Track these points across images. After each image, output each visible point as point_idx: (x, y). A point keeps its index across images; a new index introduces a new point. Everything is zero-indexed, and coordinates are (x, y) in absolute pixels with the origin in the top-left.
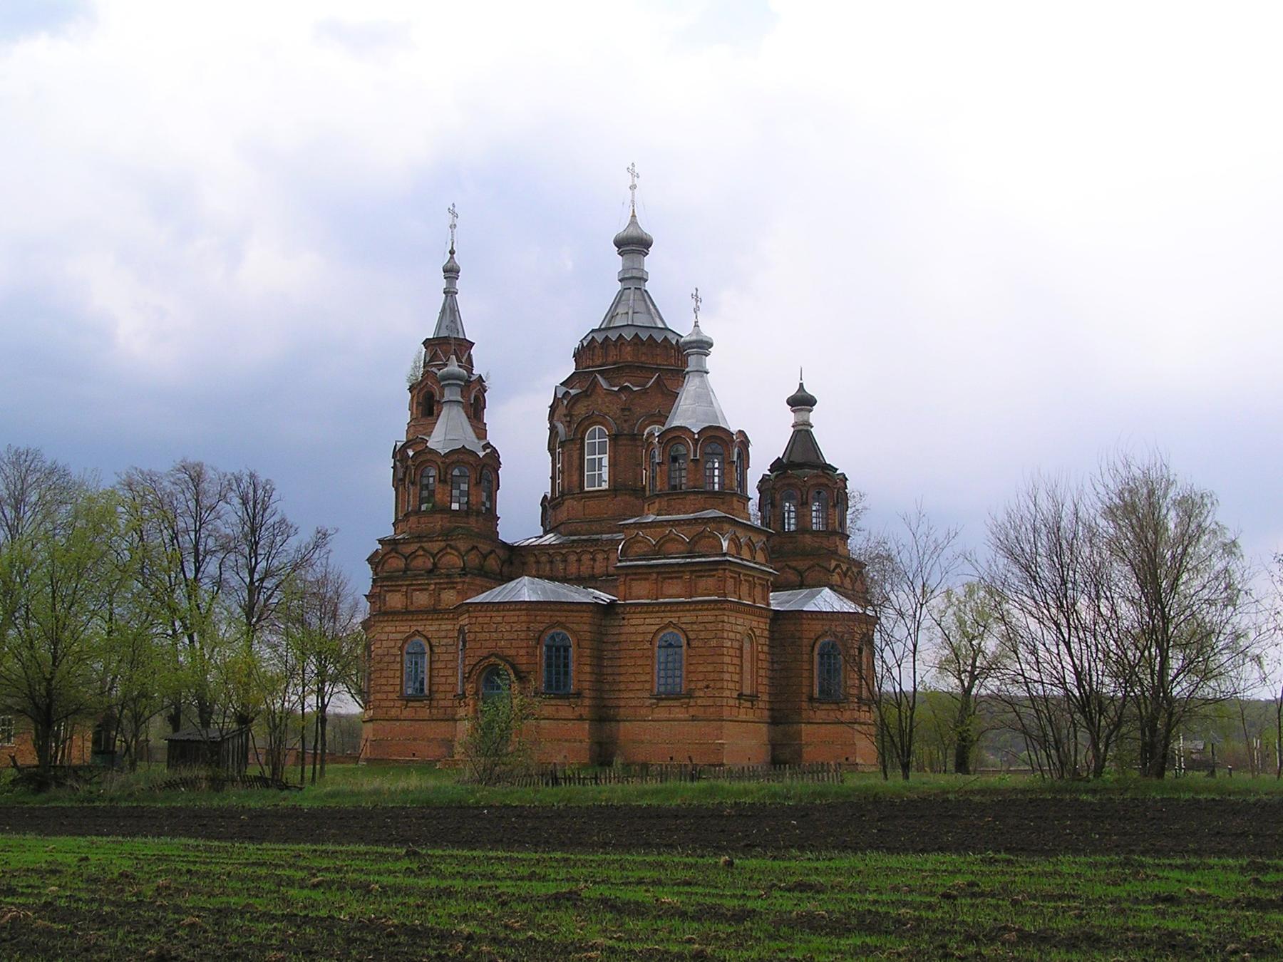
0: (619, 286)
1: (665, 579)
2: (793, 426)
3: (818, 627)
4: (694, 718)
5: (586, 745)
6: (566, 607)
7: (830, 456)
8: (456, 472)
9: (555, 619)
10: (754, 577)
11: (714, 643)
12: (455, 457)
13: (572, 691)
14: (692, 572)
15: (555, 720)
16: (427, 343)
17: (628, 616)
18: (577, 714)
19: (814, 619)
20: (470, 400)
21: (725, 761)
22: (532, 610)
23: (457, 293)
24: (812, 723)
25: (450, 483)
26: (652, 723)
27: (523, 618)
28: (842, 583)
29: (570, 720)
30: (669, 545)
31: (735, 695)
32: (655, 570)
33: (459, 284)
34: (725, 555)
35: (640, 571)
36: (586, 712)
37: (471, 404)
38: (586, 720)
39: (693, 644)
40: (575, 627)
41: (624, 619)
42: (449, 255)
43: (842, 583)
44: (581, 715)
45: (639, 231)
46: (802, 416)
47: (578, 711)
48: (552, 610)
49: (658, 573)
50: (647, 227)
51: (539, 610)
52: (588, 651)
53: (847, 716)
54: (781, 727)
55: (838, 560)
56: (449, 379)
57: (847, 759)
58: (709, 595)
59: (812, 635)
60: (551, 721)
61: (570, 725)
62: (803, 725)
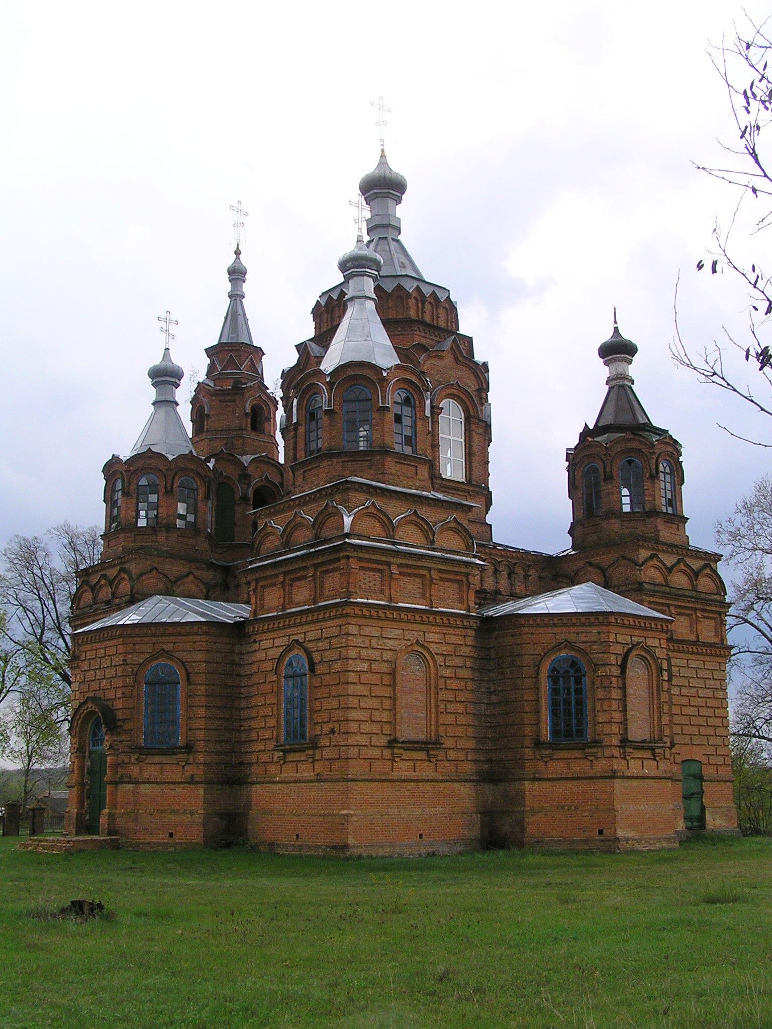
2: (607, 384)
3: (547, 637)
4: (319, 779)
5: (198, 819)
8: (143, 481)
10: (429, 569)
11: (337, 666)
12: (140, 464)
13: (180, 744)
14: (316, 566)
15: (157, 783)
16: (210, 351)
18: (188, 774)
19: (539, 626)
21: (351, 841)
23: (244, 297)
25: (134, 495)
27: (121, 649)
28: (666, 580)
30: (297, 533)
31: (384, 741)
33: (246, 287)
34: (347, 535)
35: (267, 573)
36: (199, 772)
37: (246, 414)
38: (200, 783)
39: (320, 669)
40: (186, 657)
41: (255, 641)
42: (235, 256)
43: (666, 580)
44: (192, 777)
45: (387, 171)
46: (620, 367)
47: (190, 770)
48: (154, 635)
49: (285, 573)
50: (398, 167)
51: (138, 636)
52: (203, 687)
53: (601, 766)
54: (502, 786)
55: (653, 549)
56: (165, 375)
57: (601, 832)
58: (447, 608)
60: (377, 783)
61: (179, 790)
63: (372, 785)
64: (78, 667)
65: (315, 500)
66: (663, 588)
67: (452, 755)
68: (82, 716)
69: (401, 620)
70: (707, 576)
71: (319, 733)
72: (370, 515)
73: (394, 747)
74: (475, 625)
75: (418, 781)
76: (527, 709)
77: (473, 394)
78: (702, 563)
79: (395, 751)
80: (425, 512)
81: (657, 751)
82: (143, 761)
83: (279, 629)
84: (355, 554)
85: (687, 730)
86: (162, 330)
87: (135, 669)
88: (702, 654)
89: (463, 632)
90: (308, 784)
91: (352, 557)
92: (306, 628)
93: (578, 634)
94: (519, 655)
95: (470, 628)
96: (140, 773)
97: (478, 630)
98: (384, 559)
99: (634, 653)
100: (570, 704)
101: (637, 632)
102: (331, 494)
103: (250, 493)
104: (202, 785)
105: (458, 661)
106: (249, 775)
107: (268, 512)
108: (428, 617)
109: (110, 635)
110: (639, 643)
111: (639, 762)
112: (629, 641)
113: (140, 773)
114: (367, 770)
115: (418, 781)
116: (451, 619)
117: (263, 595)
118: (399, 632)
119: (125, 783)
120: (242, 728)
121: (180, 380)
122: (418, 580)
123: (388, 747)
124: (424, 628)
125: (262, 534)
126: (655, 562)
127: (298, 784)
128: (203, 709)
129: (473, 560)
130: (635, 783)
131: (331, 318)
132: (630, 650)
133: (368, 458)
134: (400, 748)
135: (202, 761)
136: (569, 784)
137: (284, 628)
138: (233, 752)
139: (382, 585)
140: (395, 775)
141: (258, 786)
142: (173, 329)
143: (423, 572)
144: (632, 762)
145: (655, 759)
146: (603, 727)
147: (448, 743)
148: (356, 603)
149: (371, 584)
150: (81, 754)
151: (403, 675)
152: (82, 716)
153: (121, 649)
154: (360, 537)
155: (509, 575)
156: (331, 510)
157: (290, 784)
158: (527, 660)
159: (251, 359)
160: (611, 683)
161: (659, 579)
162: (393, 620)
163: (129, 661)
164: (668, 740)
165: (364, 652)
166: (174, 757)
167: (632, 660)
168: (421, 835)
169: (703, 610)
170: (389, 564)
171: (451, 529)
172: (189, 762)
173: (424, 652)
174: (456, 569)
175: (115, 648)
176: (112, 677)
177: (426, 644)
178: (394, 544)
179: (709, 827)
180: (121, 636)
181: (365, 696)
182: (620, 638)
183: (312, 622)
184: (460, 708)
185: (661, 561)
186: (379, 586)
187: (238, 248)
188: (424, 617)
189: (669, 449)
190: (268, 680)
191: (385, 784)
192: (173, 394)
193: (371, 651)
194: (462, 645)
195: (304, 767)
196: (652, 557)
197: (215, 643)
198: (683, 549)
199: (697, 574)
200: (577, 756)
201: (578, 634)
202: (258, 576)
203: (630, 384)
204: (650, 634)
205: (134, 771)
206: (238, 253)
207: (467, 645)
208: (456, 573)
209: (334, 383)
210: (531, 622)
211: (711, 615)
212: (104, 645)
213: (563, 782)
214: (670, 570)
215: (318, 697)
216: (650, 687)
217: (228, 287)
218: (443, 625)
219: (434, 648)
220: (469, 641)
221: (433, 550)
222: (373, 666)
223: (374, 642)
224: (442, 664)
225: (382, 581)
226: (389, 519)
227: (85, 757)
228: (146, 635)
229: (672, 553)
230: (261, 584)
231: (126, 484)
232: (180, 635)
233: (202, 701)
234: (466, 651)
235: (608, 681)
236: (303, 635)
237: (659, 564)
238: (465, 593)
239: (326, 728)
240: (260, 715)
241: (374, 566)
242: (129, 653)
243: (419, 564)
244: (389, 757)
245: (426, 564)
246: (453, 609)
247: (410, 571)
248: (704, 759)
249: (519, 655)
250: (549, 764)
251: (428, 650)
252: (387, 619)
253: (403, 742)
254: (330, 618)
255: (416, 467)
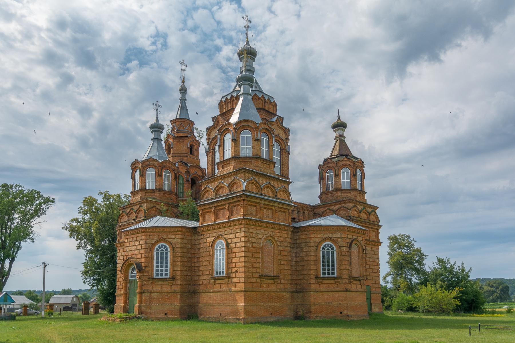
0: (335, 141)
1: (218, 210)
6: (166, 229)
7: (355, 152)
9: (160, 237)
10: (275, 206)
14: (229, 204)
17: (203, 233)
20: (187, 146)
22: (148, 232)
24: (318, 292)
26: (213, 293)
27: (144, 237)
28: (359, 216)
29: (169, 293)
31: (257, 275)
32: (213, 205)
36: (178, 290)
38: (178, 293)
40: (172, 241)
41: (201, 235)
43: (359, 216)
51: (151, 232)
55: (355, 203)
57: (341, 313)
59: (317, 240)
60: (254, 293)
61: (169, 296)
62: (312, 293)
63: (252, 293)
64: (124, 246)
65: (229, 177)
66: (358, 219)
67: (283, 281)
68: (126, 265)
69: (264, 227)
70: (373, 215)
71: (231, 272)
72: (252, 183)
73: (261, 278)
74: (291, 230)
75: (270, 292)
76: (312, 264)
77: (285, 140)
78: (371, 210)
79: (262, 279)
80: (273, 183)
81: (361, 281)
82: (153, 284)
83: (212, 229)
84: (247, 199)
85: (371, 274)
86: (155, 109)
87: (150, 246)
88: (371, 245)
89: (287, 232)
90: (225, 293)
91: (246, 200)
92: (225, 229)
93: (333, 234)
94: (309, 242)
95: (290, 231)
96: (152, 289)
97: (292, 232)
98: (258, 201)
99: (354, 242)
100: (329, 262)
101: (354, 234)
102: (236, 174)
103: (190, 179)
104: (179, 294)
105: (285, 244)
106: (199, 289)
107: (207, 182)
108: (274, 225)
109: (139, 231)
110: (355, 239)
111: (355, 285)
112: (352, 237)
113: (152, 289)
114: (251, 287)
115: (270, 292)
116: (283, 227)
117: (205, 216)
118: (263, 231)
119: (146, 293)
120: (195, 270)
121: (163, 130)
122: (270, 211)
123: (259, 278)
124: (273, 230)
125: (205, 191)
126: (355, 208)
127: (221, 293)
128: (180, 262)
129: (291, 204)
130: (354, 293)
131: (227, 107)
132: (352, 241)
133: (251, 160)
134: (264, 278)
135: (179, 283)
136: (329, 293)
137: (215, 229)
138: (192, 280)
139: (257, 212)
140: (261, 289)
141: (203, 294)
142: (159, 109)
143: (272, 208)
144: (353, 285)
145: (361, 284)
146: (342, 271)
147: (282, 277)
148: (247, 219)
149: (253, 212)
150: (125, 281)
151: (264, 249)
152: (126, 265)
153: (144, 237)
154: (249, 192)
155: (298, 212)
156: (236, 181)
157: (217, 293)
158: (312, 244)
159: (189, 126)
160: (346, 254)
161: (357, 215)
162: (262, 226)
163: (147, 242)
164: (365, 277)
165: (250, 239)
166: (167, 282)
167: (353, 245)
168: (271, 313)
169: (372, 228)
170: (259, 204)
171: (283, 191)
172: (173, 284)
173: (273, 240)
174: (284, 207)
175: (141, 237)
176: (140, 249)
177: (273, 237)
178: (262, 195)
179: (373, 311)
180: (144, 232)
181: (250, 257)
182: (349, 236)
183: (228, 227)
184: (286, 263)
185: (357, 208)
186: (255, 212)
187: (183, 80)
188: (273, 225)
189: (360, 165)
190: (207, 251)
191: (258, 293)
192: (160, 136)
193: (253, 239)
194: (286, 238)
195: (224, 286)
196: (354, 207)
197: (184, 235)
198: (364, 203)
199: (370, 214)
200: (332, 283)
201: (333, 234)
202: (203, 208)
203: (344, 139)
204: (359, 235)
205: (150, 288)
206: (183, 82)
207: (288, 238)
208: (285, 209)
209: (236, 128)
210: (314, 229)
211: (374, 230)
212: (136, 236)
213: (327, 293)
214: (360, 212)
215: (230, 257)
216: (359, 256)
217: (180, 96)
218: (280, 229)
219: (276, 238)
220: (289, 236)
221: (276, 199)
222: (253, 245)
223: (254, 235)
224: (279, 245)
225: (257, 210)
226: (260, 185)
227: (127, 282)
228: (155, 232)
229: (361, 205)
230: (204, 211)
231: (142, 171)
232: (170, 232)
233: (179, 259)
234: (288, 240)
235: (345, 253)
236: (223, 232)
237: (356, 209)
238: (288, 217)
239: (234, 270)
240: (204, 265)
241: (254, 204)
242: (147, 239)
243: (271, 204)
244: (259, 282)
245: (273, 204)
246: (283, 223)
247: (268, 207)
248: (371, 285)
249: (309, 242)
250: (321, 286)
251: (274, 239)
252: (259, 226)
253: (265, 276)
254: (236, 225)
255: (269, 165)
